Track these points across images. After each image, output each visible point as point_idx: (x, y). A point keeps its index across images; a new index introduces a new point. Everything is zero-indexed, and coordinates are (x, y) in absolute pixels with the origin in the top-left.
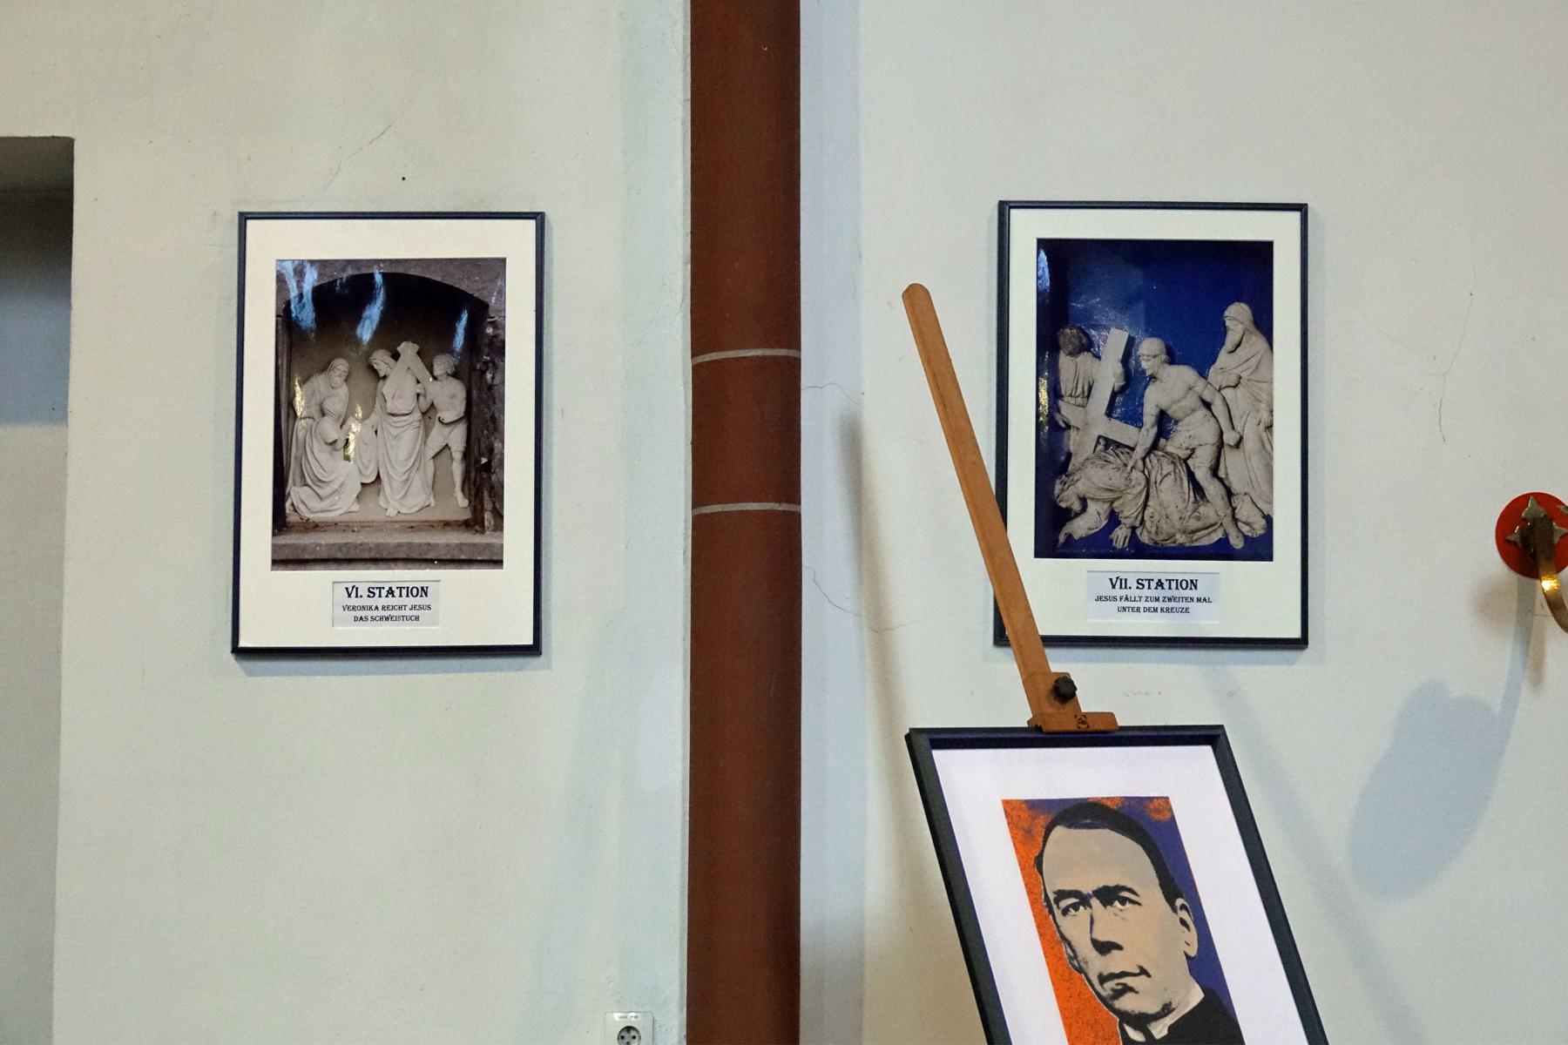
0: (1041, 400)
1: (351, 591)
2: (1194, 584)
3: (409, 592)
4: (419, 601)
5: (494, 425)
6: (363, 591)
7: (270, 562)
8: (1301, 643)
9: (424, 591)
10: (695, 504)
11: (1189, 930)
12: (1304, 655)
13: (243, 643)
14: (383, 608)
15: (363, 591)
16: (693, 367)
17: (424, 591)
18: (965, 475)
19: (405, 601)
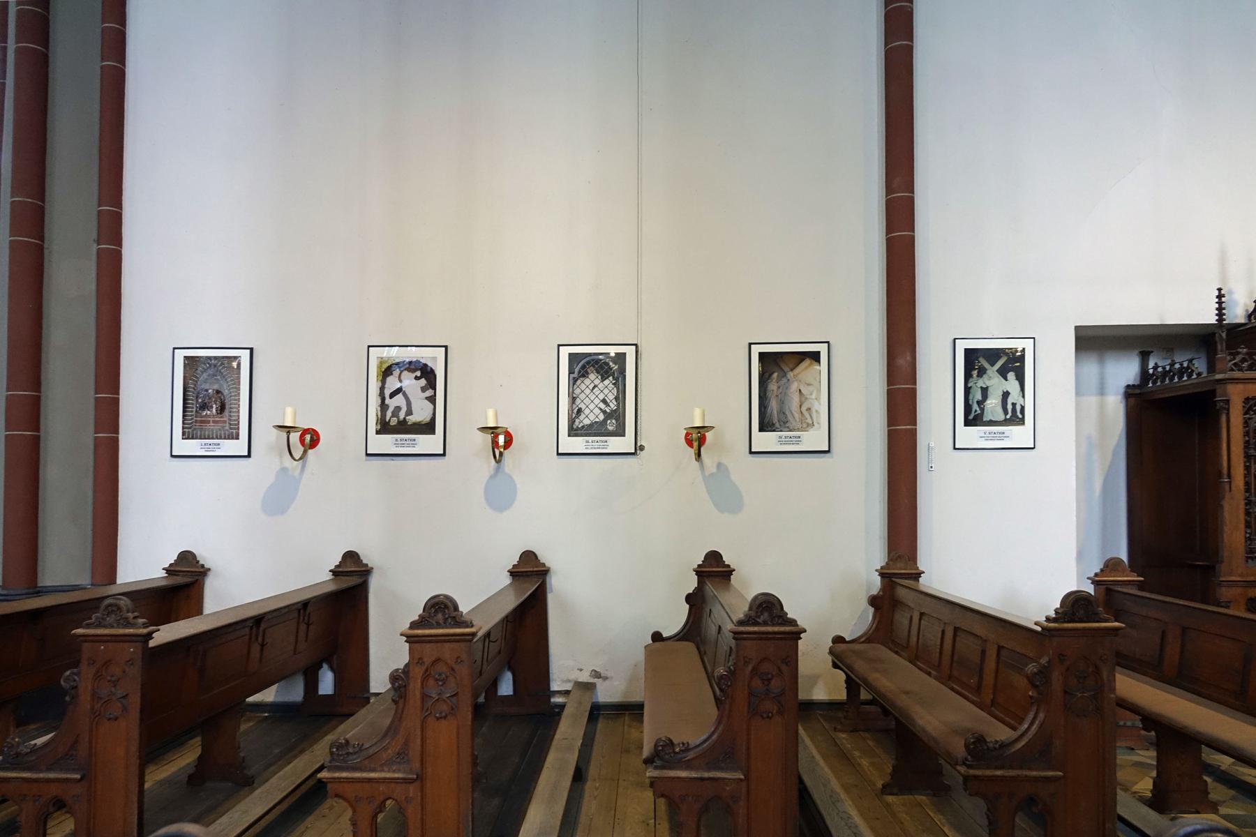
0: (258, 648)
1: (780, 437)
2: (1003, 433)
3: (795, 437)
4: (218, 447)
5: (760, 397)
6: (399, 440)
7: (375, 431)
8: (251, 349)
9: (799, 437)
10: (888, 426)
11: (159, 630)
12: (1034, 450)
13: (368, 452)
14: (205, 445)
15: (399, 440)
16: (886, 201)
17: (414, 440)
18: (576, 818)
19: (998, 435)
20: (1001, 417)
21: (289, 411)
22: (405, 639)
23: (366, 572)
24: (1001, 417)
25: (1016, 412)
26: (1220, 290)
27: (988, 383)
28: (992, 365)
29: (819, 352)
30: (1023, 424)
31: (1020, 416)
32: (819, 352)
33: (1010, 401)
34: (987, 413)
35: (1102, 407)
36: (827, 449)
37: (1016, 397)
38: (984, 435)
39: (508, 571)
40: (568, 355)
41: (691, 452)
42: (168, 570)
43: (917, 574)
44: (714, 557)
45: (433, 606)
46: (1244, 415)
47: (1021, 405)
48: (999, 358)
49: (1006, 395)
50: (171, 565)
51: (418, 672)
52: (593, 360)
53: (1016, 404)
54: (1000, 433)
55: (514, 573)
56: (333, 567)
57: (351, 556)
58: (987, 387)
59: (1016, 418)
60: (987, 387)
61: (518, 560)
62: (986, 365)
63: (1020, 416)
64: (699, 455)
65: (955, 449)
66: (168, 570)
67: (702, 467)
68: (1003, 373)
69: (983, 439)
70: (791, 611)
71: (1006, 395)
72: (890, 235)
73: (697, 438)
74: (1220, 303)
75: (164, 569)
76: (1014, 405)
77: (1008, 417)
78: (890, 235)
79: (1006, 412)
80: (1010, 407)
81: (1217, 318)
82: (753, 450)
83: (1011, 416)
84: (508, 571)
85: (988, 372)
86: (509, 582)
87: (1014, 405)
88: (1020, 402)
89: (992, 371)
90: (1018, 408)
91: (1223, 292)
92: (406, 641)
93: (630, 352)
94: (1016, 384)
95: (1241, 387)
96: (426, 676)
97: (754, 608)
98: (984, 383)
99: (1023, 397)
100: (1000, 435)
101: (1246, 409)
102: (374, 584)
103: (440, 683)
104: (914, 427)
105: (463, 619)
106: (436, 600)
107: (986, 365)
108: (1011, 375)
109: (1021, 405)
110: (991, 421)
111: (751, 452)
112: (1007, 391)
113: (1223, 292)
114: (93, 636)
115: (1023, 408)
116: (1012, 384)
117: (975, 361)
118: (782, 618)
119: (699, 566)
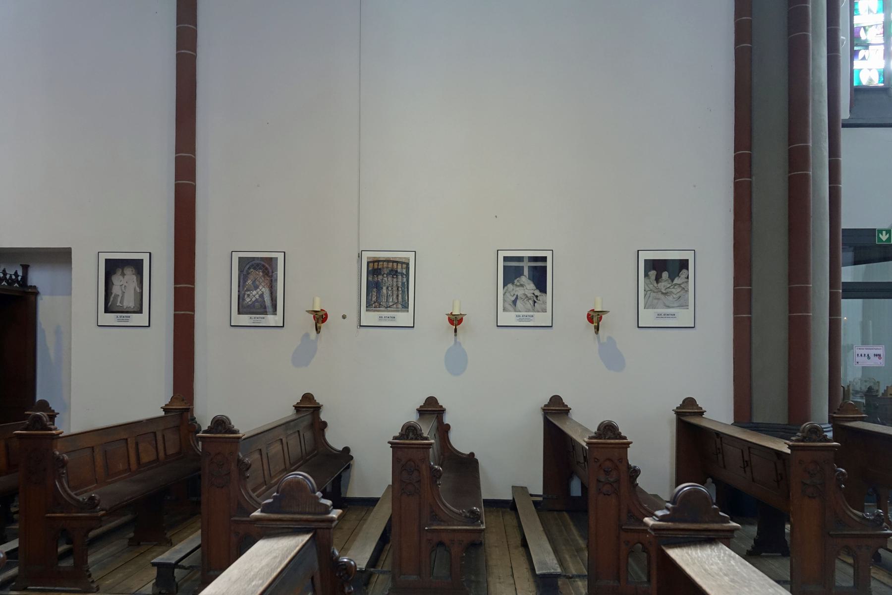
8: (284, 252)
12: (284, 328)
15: (521, 316)
21: (317, 300)
22: (788, 446)
39: (294, 406)
40: (104, 260)
41: (592, 327)
43: (566, 410)
44: (556, 400)
52: (255, 264)
54: (392, 317)
55: (298, 408)
56: (295, 404)
61: (170, 401)
64: (456, 331)
67: (598, 338)
70: (623, 431)
73: (595, 318)
75: (161, 408)
84: (417, 410)
86: (291, 414)
92: (391, 447)
93: (280, 257)
97: (602, 429)
104: (177, 312)
106: (214, 421)
111: (638, 327)
114: (417, 444)
117: (113, 267)
118: (619, 436)
119: (545, 406)
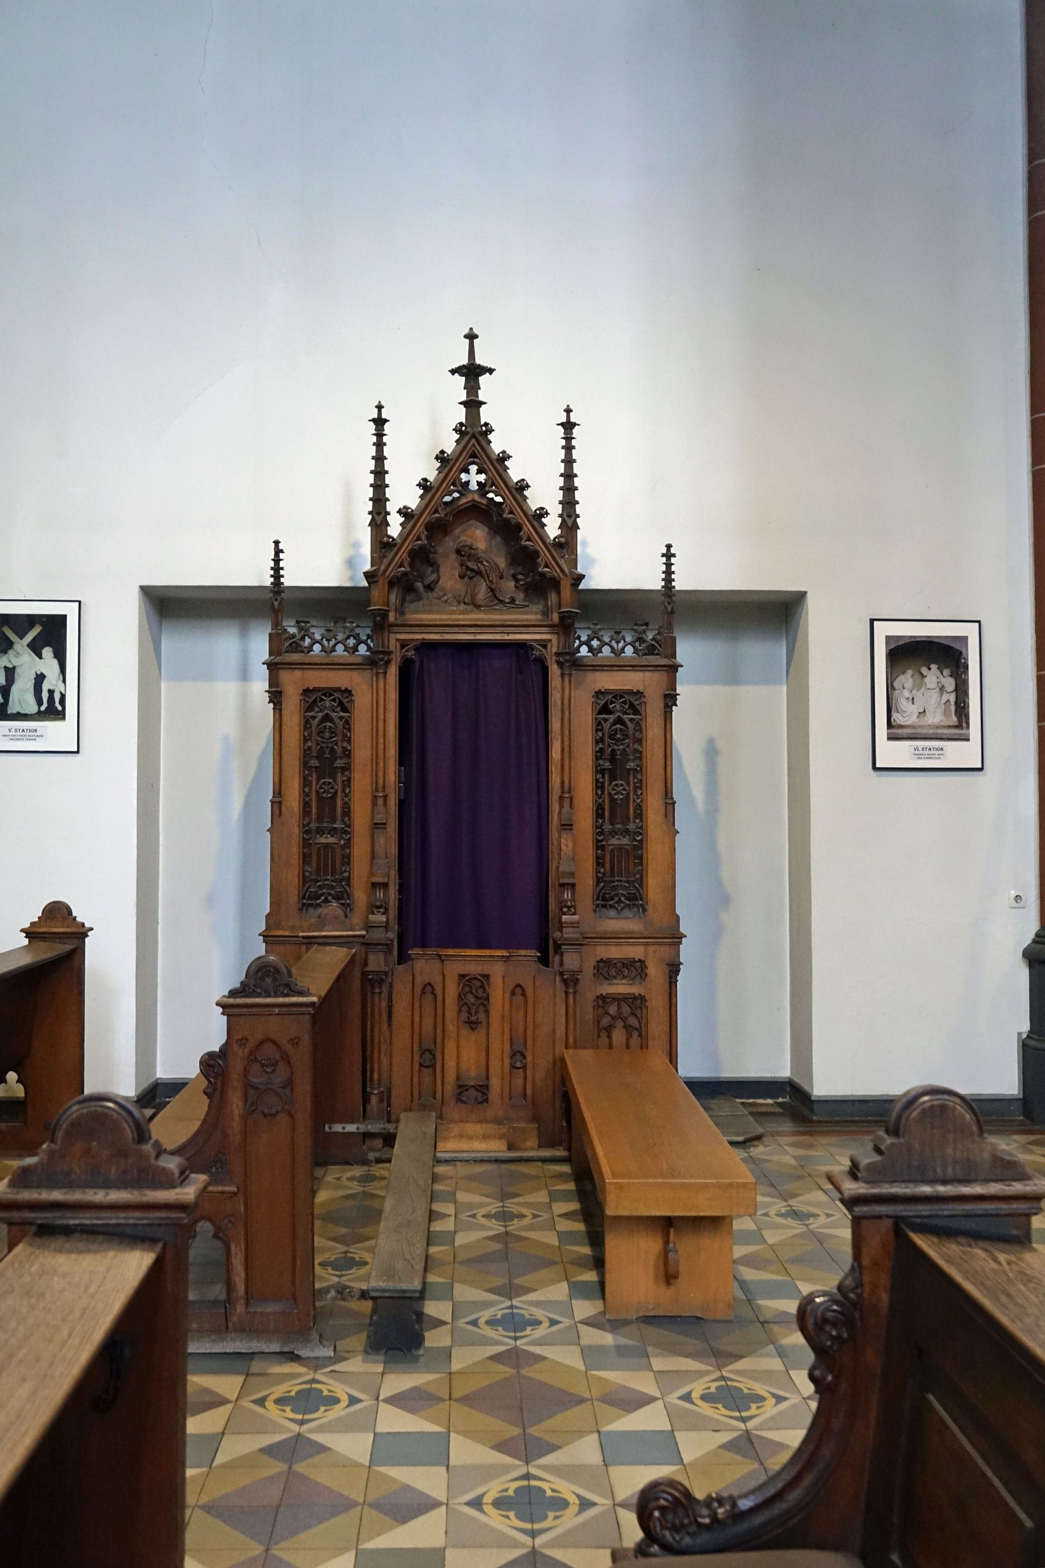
5: (966, 694)
9: (942, 749)
19: (28, 734)
20: (32, 708)
23: (81, 934)
24: (32, 708)
25: (54, 702)
26: (669, 547)
27: (16, 662)
28: (21, 637)
29: (65, 616)
30: (64, 718)
31: (60, 708)
32: (65, 616)
33: (46, 686)
34: (13, 702)
35: (244, 697)
36: (980, 766)
37: (54, 682)
38: (8, 733)
42: (30, 933)
45: (259, 970)
46: (598, 714)
47: (61, 693)
48: (32, 626)
49: (40, 678)
50: (33, 924)
51: (240, 1053)
53: (54, 691)
57: (57, 911)
58: (14, 667)
59: (53, 711)
60: (14, 667)
62: (12, 636)
63: (60, 708)
65: (78, 752)
66: (30, 933)
68: (36, 648)
69: (8, 738)
71: (40, 678)
72: (1038, 467)
74: (669, 565)
75: (22, 931)
76: (51, 692)
77: (43, 708)
78: (1038, 467)
79: (40, 703)
80: (45, 696)
81: (272, 580)
82: (878, 766)
83: (46, 708)
85: (15, 646)
87: (51, 692)
88: (59, 688)
89: (21, 645)
90: (57, 697)
91: (673, 551)
93: (883, 630)
94: (55, 663)
95: (298, 674)
96: (252, 1058)
98: (10, 661)
99: (64, 681)
100: (31, 734)
101: (307, 705)
102: (90, 943)
103: (269, 1070)
105: (297, 987)
107: (12, 636)
108: (47, 652)
109: (61, 693)
110: (19, 714)
112: (42, 673)
113: (673, 551)
115: (63, 697)
116: (48, 663)
